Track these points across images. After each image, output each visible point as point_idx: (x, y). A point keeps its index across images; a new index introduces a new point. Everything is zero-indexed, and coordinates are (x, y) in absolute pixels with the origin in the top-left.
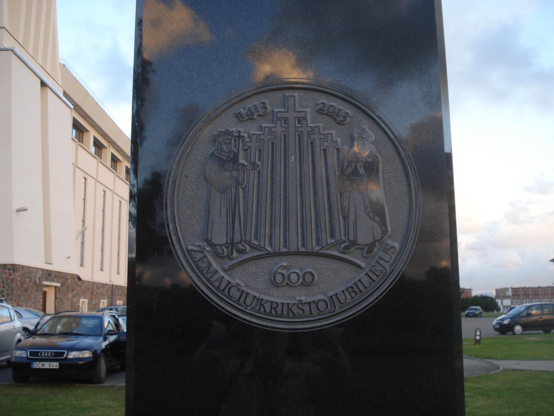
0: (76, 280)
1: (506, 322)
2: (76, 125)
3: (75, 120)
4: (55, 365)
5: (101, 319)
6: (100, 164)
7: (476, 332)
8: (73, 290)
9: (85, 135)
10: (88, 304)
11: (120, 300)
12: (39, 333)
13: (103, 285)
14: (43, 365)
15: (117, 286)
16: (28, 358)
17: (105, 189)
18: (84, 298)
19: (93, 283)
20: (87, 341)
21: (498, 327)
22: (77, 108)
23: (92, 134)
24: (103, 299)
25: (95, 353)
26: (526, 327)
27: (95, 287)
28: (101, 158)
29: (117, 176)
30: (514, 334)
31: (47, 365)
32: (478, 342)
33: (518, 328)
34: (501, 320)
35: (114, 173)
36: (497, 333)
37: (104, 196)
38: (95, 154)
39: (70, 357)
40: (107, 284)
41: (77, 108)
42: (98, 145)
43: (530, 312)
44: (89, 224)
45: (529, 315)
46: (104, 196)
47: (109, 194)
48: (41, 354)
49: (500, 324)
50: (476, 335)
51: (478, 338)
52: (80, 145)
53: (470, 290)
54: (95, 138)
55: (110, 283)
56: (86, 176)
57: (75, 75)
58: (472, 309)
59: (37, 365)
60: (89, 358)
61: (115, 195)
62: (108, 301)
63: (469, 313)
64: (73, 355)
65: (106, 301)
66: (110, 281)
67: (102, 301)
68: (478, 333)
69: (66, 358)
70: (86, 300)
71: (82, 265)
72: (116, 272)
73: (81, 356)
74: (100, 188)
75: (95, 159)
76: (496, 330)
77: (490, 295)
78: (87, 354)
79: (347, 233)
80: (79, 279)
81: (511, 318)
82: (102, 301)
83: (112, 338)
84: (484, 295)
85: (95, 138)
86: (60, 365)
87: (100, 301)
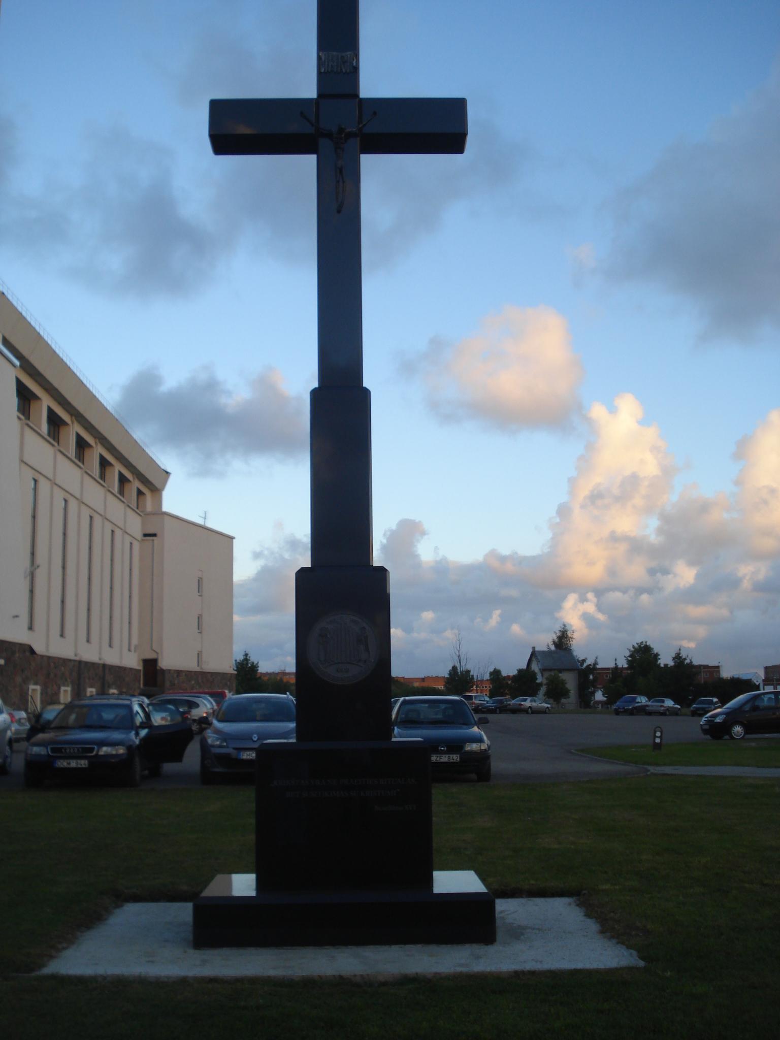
0: (28, 654)
1: (718, 720)
2: (25, 397)
3: (19, 383)
4: (84, 763)
5: (130, 707)
6: (59, 455)
7: (655, 732)
8: (23, 671)
9: (34, 406)
10: (42, 694)
11: (91, 686)
12: (53, 726)
13: (93, 665)
14: (69, 764)
15: (86, 663)
16: (49, 755)
17: (37, 476)
18: (36, 684)
19: (49, 658)
20: (117, 736)
21: (707, 727)
22: (27, 366)
23: (74, 429)
24: (64, 685)
25: (130, 748)
26: (748, 729)
27: (52, 665)
28: (28, 418)
29: (86, 473)
30: (732, 738)
31: (73, 764)
32: (657, 747)
33: (738, 729)
34: (712, 716)
35: (53, 445)
36: (708, 737)
37: (65, 509)
38: (49, 434)
39: (101, 753)
40: (70, 660)
41: (27, 366)
42: (55, 422)
43: (756, 704)
44: (41, 558)
45: (755, 708)
46: (65, 509)
47: (73, 505)
48: (66, 749)
49: (710, 722)
50: (655, 737)
51: (658, 740)
52: (28, 425)
53: (718, 667)
54: (50, 411)
55: (77, 658)
56: (37, 476)
57: (20, 309)
58: (704, 702)
59: (62, 764)
60: (122, 754)
61: (55, 488)
62: (73, 690)
63: (697, 709)
64: (105, 750)
65: (69, 689)
66: (76, 655)
67: (63, 688)
68: (658, 734)
69: (97, 755)
70: (38, 688)
71: (31, 628)
72: (85, 639)
73: (114, 752)
74: (59, 496)
75: (77, 469)
76: (705, 732)
77: (284, 673)
78: (121, 750)
79: (276, 713)
80: (32, 651)
81: (727, 714)
82: (63, 688)
83: (144, 733)
84: (736, 676)
85: (78, 436)
86: (90, 763)
87: (59, 689)
